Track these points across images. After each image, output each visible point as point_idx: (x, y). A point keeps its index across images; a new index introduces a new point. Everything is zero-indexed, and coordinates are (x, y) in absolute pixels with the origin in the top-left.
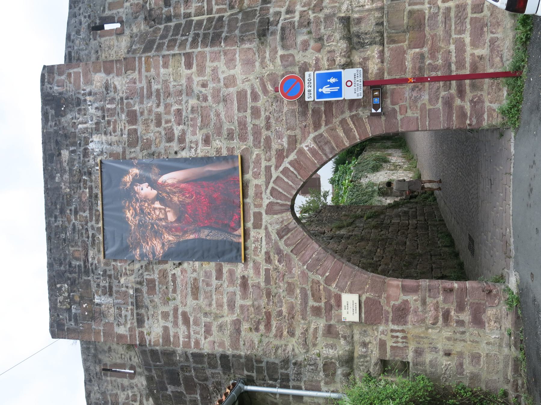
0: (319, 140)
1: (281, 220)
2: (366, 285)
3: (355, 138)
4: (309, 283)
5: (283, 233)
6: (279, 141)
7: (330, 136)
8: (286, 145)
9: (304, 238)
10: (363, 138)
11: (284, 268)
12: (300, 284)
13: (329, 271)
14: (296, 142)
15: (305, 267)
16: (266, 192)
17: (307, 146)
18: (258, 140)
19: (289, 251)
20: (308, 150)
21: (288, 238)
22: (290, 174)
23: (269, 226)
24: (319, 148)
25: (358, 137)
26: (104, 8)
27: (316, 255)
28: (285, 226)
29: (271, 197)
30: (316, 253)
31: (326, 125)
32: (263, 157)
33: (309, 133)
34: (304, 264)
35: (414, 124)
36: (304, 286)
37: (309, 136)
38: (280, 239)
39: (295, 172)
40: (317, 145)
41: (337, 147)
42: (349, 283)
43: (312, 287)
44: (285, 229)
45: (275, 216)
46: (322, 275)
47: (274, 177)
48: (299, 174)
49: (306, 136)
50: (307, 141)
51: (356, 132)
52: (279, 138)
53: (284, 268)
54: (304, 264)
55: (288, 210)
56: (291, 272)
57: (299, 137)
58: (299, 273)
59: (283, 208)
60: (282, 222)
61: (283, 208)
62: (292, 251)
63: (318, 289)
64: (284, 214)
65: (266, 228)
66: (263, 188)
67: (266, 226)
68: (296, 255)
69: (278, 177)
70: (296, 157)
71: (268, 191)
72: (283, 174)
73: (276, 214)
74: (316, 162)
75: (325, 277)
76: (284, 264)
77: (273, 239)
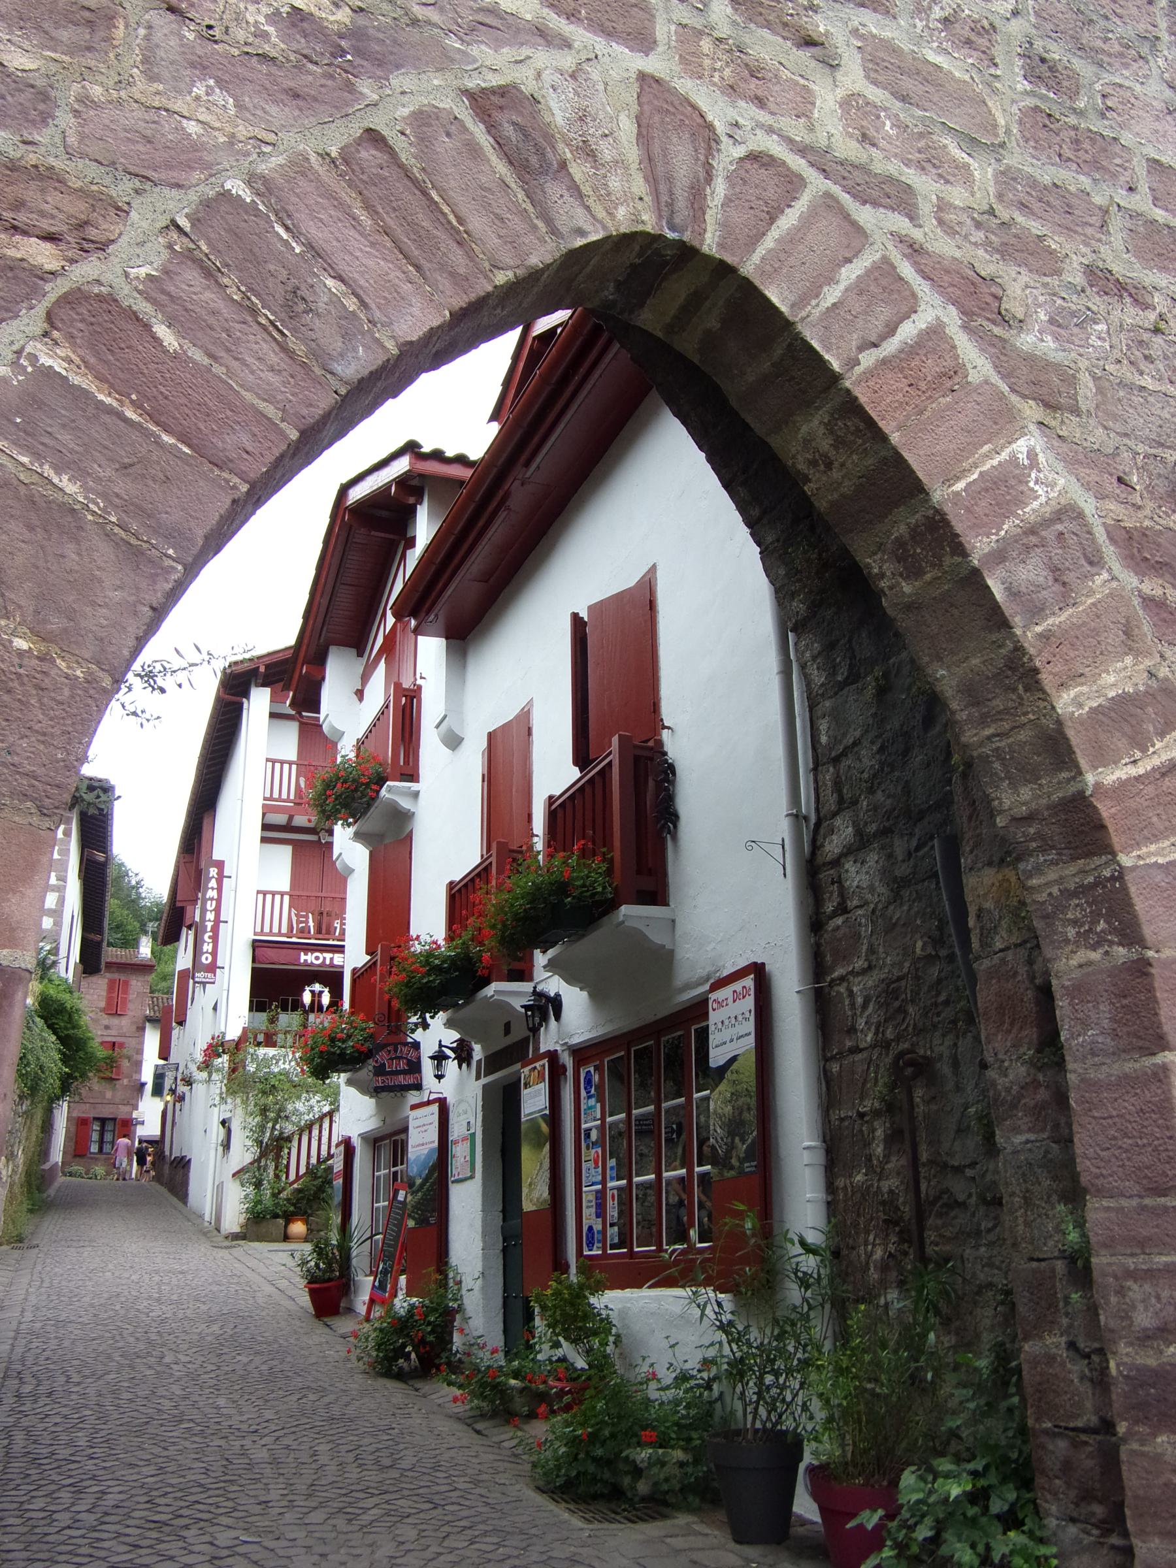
0: (1072, 540)
1: (606, 152)
2: (38, 634)
3: (1104, 758)
4: (93, 171)
5: (509, 131)
6: (1043, 316)
7: (1096, 611)
8: (1027, 341)
9: (471, 255)
10: (1106, 810)
11: (240, 34)
12: (85, 99)
13: (197, 355)
14: (1047, 405)
15: (236, 186)
16: (770, 130)
17: (1032, 455)
18: (1036, 206)
19: (378, 122)
20: (1013, 460)
21: (473, 150)
22: (884, 313)
23: (568, 61)
24: (1032, 531)
25: (1112, 776)
26: (1059, 326)
27: (335, 300)
28: (563, 165)
29: (739, 152)
30: (351, 304)
31: (1148, 602)
32: (958, 195)
33: (1100, 497)
34: (261, 184)
35: (92, 63)
36: (64, 119)
37: (1087, 487)
38: (466, 92)
39: (891, 346)
40: (1047, 522)
41: (1045, 637)
42: (70, 486)
43: (46, 176)
44: (542, 154)
45: (627, 128)
46: (154, 288)
47: (865, 215)
48: (884, 362)
49: (1083, 471)
50: (1060, 466)
51: (1133, 771)
52: (1052, 321)
53: (240, 34)
54: (261, 184)
55: (665, 208)
56: (201, 67)
57: (1071, 427)
58: (192, 128)
59: (681, 203)
60: (588, 152)
61: (681, 203)
62: (373, 137)
63: (22, 218)
64: (639, 186)
65: (543, 34)
66: (798, 132)
67: (566, 44)
68: (346, 156)
69: (857, 233)
70: (974, 377)
71: (777, 148)
72: (875, 267)
73: (644, 136)
74: (960, 486)
75: (143, 307)
76: (275, 44)
77: (474, 51)
